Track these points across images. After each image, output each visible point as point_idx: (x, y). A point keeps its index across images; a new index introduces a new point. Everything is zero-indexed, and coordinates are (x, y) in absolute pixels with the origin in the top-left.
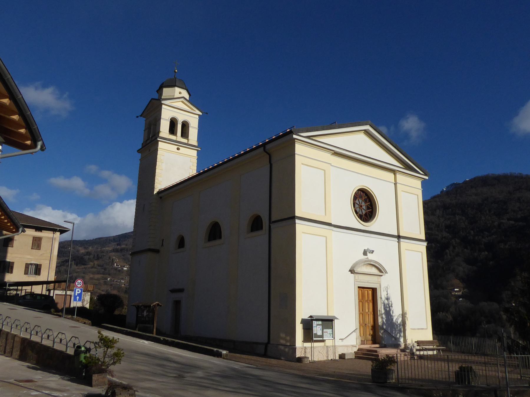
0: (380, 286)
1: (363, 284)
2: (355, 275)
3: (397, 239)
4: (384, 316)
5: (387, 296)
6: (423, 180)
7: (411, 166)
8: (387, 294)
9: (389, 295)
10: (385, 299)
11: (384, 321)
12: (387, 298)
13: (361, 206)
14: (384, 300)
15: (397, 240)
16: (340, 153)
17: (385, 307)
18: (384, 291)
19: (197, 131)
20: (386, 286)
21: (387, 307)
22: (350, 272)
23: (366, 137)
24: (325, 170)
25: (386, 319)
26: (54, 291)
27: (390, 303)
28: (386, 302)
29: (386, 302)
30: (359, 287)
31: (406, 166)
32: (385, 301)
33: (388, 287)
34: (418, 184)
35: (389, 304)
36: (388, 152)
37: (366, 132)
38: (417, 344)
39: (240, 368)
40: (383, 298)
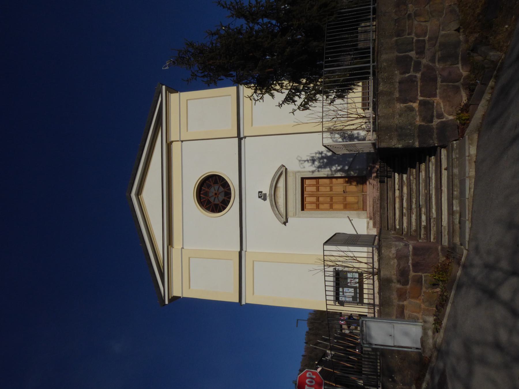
0: (299, 172)
1: (297, 202)
2: (289, 217)
3: (242, 141)
4: (334, 168)
5: (310, 161)
6: (167, 91)
7: (157, 114)
8: (308, 161)
9: (309, 159)
10: (314, 166)
11: (339, 168)
12: (312, 161)
13: (216, 194)
14: (315, 167)
15: (243, 139)
16: (168, 199)
17: (323, 165)
18: (304, 167)
19: (182, 94)
20: (298, 162)
21: (323, 162)
22: (287, 224)
23: (144, 192)
24: (187, 100)
25: (337, 165)
26: (372, 289)
27: (318, 155)
28: (317, 163)
29: (317, 163)
30: (303, 209)
31: (159, 127)
32: (316, 166)
33: (299, 159)
34: (174, 97)
35: (320, 159)
36: (151, 155)
37: (139, 193)
38: (366, 110)
39: (446, 120)
40: (313, 168)
